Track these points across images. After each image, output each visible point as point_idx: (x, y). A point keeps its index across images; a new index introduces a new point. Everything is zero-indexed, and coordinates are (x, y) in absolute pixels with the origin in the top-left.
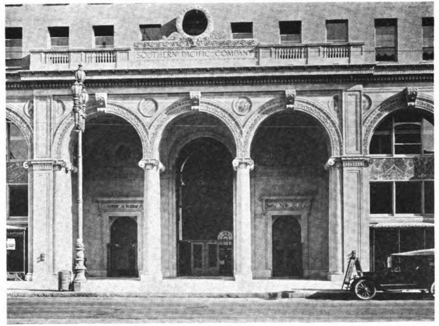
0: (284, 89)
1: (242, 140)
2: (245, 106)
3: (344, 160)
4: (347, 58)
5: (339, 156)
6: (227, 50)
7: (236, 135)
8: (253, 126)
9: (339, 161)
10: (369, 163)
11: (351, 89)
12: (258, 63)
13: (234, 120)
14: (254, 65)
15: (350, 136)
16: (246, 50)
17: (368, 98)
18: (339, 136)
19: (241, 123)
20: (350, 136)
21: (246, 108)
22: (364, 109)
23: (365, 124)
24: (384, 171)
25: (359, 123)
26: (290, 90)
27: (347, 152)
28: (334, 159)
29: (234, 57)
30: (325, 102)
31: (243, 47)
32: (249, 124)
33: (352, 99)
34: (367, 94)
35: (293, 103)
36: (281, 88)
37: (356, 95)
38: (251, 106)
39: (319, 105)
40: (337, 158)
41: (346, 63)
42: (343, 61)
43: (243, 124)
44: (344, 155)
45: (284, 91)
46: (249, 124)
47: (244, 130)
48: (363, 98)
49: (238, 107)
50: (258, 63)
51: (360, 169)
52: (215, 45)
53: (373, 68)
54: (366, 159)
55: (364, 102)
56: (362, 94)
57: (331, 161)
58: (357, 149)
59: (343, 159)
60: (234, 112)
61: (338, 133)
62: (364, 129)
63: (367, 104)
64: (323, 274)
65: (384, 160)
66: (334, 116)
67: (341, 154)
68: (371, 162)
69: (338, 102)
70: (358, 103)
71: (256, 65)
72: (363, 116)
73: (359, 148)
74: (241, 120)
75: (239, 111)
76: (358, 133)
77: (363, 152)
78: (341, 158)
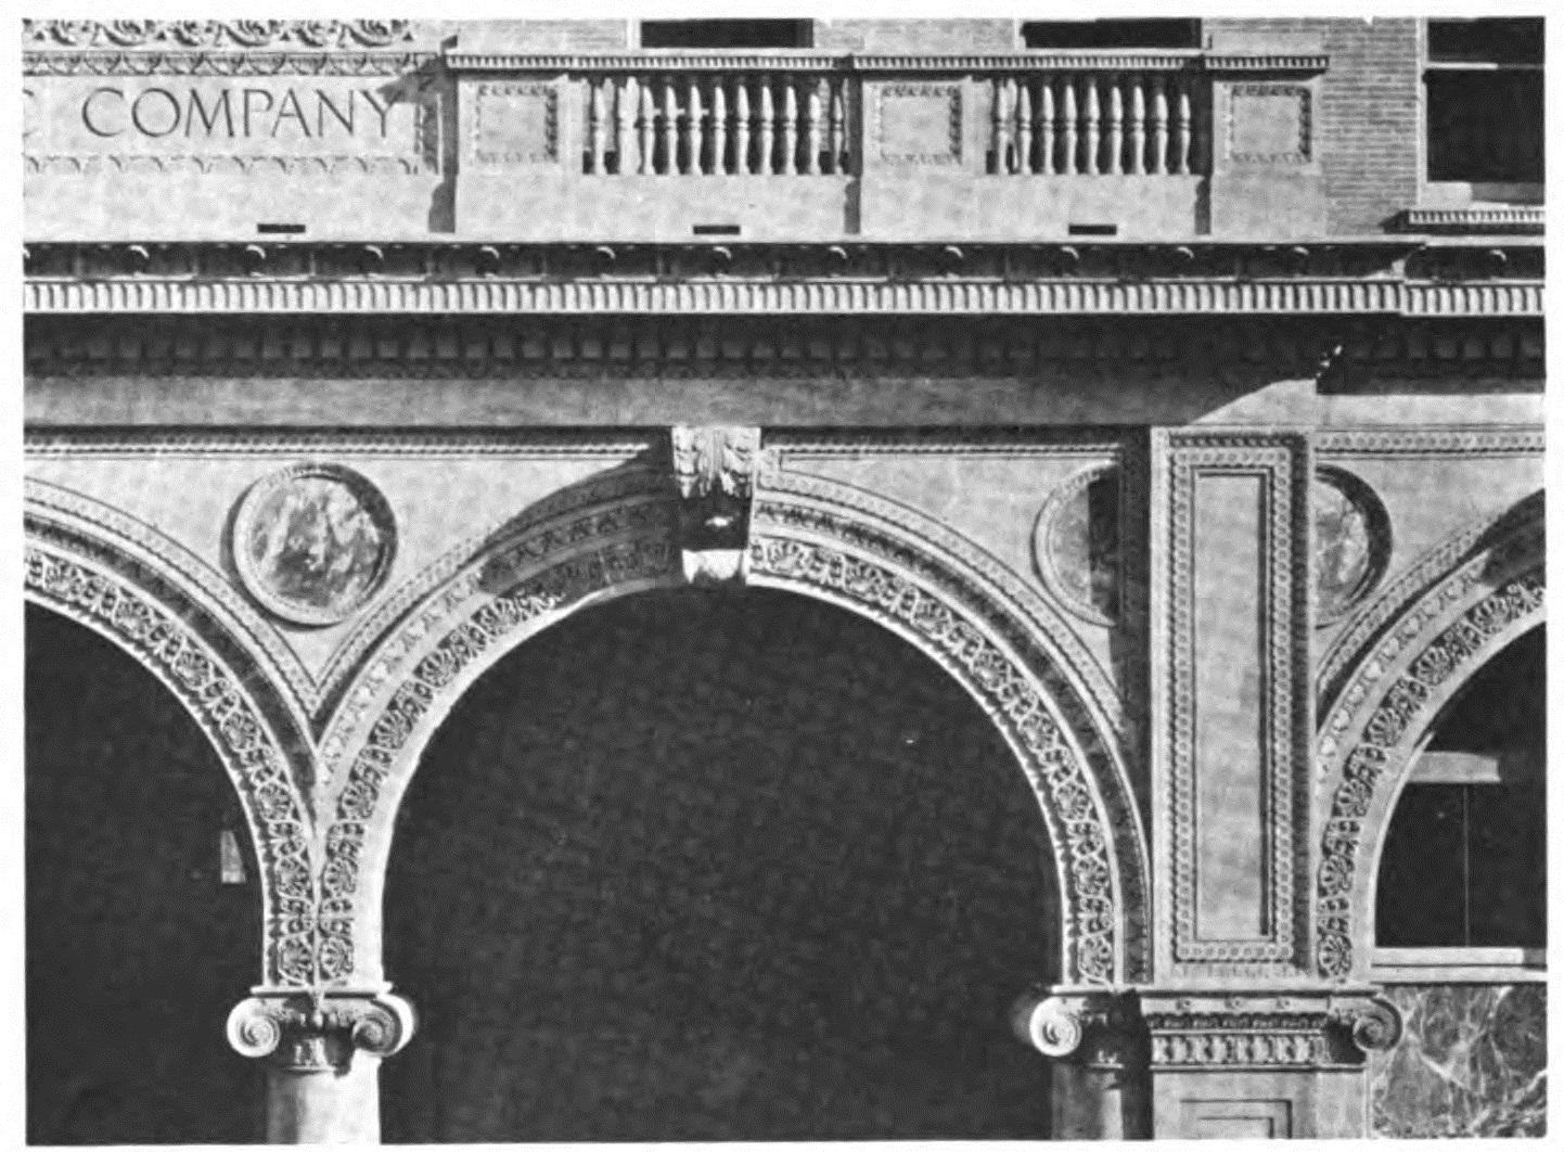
0: (653, 418)
1: (313, 838)
2: (335, 549)
3: (1160, 1019)
4: (1187, 183)
5: (1119, 985)
6: (182, 87)
7: (256, 772)
8: (402, 711)
9: (1120, 1027)
10: (1365, 1036)
11: (1217, 419)
12: (444, 206)
13: (243, 663)
14: (418, 230)
15: (1204, 801)
16: (340, 88)
17: (1354, 489)
18: (1120, 818)
19: (301, 707)
20: (1204, 801)
21: (343, 563)
22: (1330, 585)
23: (1339, 716)
24: (1494, 1096)
25: (1289, 702)
26: (714, 439)
27: (1188, 948)
28: (1077, 1005)
29: (240, 146)
30: (999, 509)
31: (319, 63)
32: (364, 707)
33: (1230, 502)
34: (1348, 465)
35: (736, 538)
36: (637, 404)
37: (1266, 481)
38: (386, 550)
39: (962, 529)
40: (1098, 999)
41: (1179, 230)
42: (1149, 208)
43: (315, 702)
44: (1165, 974)
45: (660, 438)
46: (364, 707)
47: (334, 756)
48: (1323, 499)
49: (268, 563)
50: (444, 206)
51: (1292, 1087)
52: (83, 45)
53: (1399, 266)
54: (1338, 1006)
55: (1332, 527)
56: (1313, 460)
57: (1052, 1023)
58: (1266, 927)
59: (1147, 1006)
60: (240, 586)
61: (1110, 789)
62: (1324, 754)
63: (1356, 543)
64: (1535, 27)
65: (1503, 992)
66: (1086, 646)
67: (1138, 967)
68: (1378, 1031)
69: (1114, 524)
70: (1284, 529)
71: (433, 227)
72: (1316, 648)
73: (1284, 918)
74: (302, 662)
75: (273, 587)
76: (1281, 792)
77: (1316, 954)
78: (1132, 998)
